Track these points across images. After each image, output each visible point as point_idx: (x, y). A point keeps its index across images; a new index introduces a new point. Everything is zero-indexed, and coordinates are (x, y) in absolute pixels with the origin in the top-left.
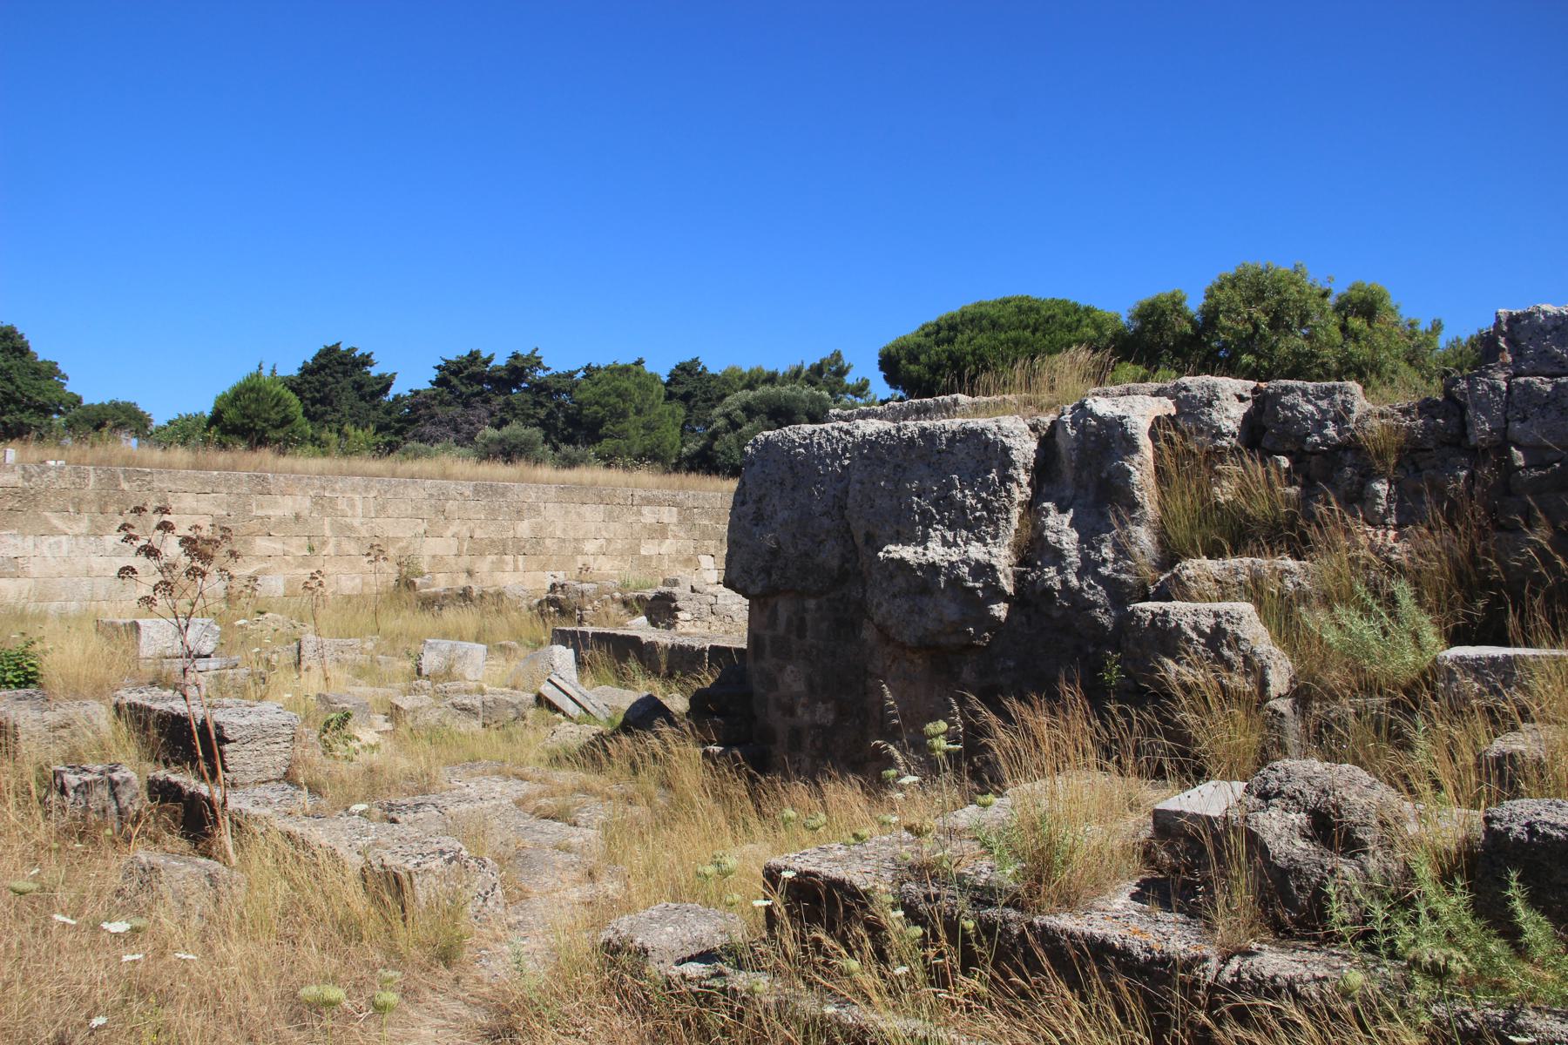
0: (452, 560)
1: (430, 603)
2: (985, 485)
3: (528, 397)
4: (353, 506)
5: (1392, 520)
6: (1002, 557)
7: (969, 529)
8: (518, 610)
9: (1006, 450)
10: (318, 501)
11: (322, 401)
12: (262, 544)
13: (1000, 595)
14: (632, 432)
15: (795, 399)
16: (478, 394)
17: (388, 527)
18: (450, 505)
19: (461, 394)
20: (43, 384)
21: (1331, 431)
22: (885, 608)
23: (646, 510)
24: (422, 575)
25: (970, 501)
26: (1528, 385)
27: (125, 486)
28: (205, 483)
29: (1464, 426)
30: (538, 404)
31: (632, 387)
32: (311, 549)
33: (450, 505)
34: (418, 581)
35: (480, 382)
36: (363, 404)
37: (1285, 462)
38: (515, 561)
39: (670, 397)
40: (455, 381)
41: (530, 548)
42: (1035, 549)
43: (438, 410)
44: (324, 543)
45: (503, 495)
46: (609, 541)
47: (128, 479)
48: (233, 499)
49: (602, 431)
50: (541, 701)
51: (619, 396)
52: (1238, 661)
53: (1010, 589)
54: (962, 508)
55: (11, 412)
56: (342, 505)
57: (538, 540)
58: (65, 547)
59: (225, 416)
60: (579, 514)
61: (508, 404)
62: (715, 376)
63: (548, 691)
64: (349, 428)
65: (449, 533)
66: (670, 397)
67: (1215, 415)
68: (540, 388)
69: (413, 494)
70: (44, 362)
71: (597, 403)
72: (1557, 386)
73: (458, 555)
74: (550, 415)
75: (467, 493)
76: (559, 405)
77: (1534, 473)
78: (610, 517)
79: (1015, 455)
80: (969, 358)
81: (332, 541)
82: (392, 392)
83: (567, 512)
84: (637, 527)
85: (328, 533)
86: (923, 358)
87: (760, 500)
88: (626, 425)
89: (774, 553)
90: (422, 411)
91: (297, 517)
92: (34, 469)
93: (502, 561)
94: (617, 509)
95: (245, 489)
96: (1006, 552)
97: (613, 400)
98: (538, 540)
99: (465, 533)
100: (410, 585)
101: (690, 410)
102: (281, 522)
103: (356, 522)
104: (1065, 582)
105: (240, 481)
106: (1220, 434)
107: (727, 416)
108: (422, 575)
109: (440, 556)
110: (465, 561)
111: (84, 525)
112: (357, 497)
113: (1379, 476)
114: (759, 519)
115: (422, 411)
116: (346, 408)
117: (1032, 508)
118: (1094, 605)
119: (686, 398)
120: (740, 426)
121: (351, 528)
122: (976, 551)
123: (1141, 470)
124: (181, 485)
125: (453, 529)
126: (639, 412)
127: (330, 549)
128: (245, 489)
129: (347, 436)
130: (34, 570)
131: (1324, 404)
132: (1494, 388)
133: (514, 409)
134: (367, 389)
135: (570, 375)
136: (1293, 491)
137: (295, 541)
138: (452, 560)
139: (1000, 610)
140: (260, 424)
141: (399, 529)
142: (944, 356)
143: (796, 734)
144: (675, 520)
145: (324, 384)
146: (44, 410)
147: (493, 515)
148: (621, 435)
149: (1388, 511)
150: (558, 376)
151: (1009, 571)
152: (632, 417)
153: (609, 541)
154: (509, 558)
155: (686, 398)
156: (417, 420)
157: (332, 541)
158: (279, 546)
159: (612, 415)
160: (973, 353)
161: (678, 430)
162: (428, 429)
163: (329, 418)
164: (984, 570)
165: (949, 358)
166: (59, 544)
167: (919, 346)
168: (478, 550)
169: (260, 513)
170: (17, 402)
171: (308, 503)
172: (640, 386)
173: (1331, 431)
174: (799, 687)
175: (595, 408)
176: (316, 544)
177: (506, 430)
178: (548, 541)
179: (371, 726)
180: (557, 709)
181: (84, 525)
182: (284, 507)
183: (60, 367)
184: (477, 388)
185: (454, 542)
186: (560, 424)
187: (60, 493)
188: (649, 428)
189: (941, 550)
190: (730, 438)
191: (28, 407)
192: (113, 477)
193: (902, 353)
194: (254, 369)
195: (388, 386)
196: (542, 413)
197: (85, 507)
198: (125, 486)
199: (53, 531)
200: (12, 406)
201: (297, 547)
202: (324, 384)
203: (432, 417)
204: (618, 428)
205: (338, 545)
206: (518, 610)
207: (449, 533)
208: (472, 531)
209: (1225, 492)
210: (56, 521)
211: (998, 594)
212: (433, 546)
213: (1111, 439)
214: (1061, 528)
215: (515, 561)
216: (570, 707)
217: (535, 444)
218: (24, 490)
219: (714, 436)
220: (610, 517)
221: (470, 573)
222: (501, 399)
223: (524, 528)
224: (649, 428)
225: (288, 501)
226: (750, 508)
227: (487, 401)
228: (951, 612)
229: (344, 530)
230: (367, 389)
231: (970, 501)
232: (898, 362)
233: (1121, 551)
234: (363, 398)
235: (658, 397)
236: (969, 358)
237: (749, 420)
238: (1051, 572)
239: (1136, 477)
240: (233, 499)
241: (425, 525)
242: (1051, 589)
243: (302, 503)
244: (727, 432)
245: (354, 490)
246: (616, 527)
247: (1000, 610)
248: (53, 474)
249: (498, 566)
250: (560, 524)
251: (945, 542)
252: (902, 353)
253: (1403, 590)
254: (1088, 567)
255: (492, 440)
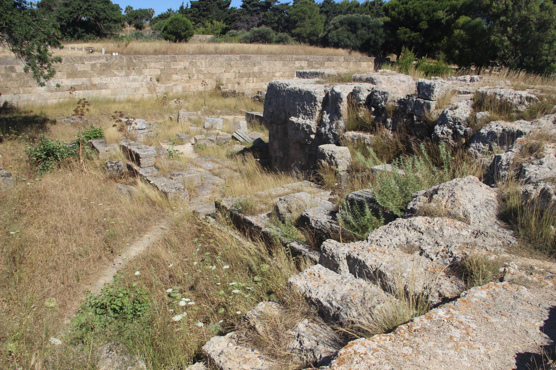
0: (233, 79)
1: (225, 95)
2: (311, 105)
3: (272, 12)
4: (202, 64)
5: (391, 128)
6: (313, 124)
7: (308, 115)
8: (248, 98)
9: (315, 98)
10: (191, 63)
11: (206, 10)
12: (175, 77)
13: (312, 133)
14: (307, 25)
15: (357, 19)
16: (256, 11)
17: (213, 70)
18: (232, 63)
19: (250, 11)
20: (115, 13)
21: (383, 104)
22: (291, 132)
23: (296, 62)
24: (223, 85)
25: (308, 109)
26: (419, 101)
27: (134, 61)
28: (157, 59)
29: (406, 108)
30: (275, 15)
31: (307, 9)
32: (189, 78)
33: (232, 63)
34: (221, 87)
35: (256, 6)
36: (221, 11)
37: (373, 109)
38: (253, 79)
39: (321, 12)
40: (248, 6)
41: (258, 76)
42: (321, 123)
43: (242, 17)
44: (193, 76)
45: (249, 59)
46: (284, 72)
47: (135, 59)
48: (165, 63)
49: (297, 25)
50: (233, 137)
51: (303, 12)
52: (334, 163)
53: (315, 132)
54: (306, 110)
55: (106, 23)
56: (198, 64)
57: (260, 73)
58: (119, 80)
59: (168, 28)
60: (274, 64)
61: (265, 15)
62: (338, 4)
63: (235, 135)
64: (215, 22)
65: (232, 71)
66: (321, 12)
67: (360, 95)
68: (276, 9)
69: (220, 60)
70: (115, 5)
71: (295, 15)
72: (424, 102)
73: (235, 78)
74: (279, 19)
75: (238, 58)
76: (282, 16)
77: (418, 123)
78: (284, 65)
79: (317, 99)
80: (411, 10)
81: (196, 75)
82: (231, 6)
83: (270, 64)
84: (293, 68)
85: (194, 72)
86: (396, 9)
87: (270, 99)
88: (304, 23)
89: (272, 113)
90: (237, 17)
91: (185, 68)
92: (109, 58)
93: (249, 80)
94: (287, 62)
95: (169, 60)
96: (315, 122)
97: (300, 14)
98: (260, 73)
99: (237, 71)
100: (219, 88)
101: (328, 17)
102: (180, 70)
103: (203, 69)
104: (325, 132)
105: (167, 58)
106: (360, 100)
107: (334, 24)
108: (223, 85)
109: (229, 78)
110: (237, 80)
111: (123, 73)
112: (203, 61)
113: (389, 117)
114: (270, 103)
115: (237, 17)
116: (214, 13)
117: (322, 113)
118: (330, 139)
119: (326, 12)
120: (338, 28)
121: (201, 71)
122: (308, 122)
123: (344, 107)
124: (150, 60)
125: (233, 70)
126: (310, 18)
127: (195, 77)
128: (169, 60)
129: (214, 24)
130: (111, 86)
131: (383, 96)
132: (413, 100)
133: (267, 17)
134: (222, 5)
135: (287, 4)
136: (374, 117)
137: (185, 75)
138: (233, 79)
139: (313, 136)
140: (179, 31)
141: (217, 70)
142: (403, 9)
143: (276, 157)
144: (306, 65)
145: (207, 5)
146: (116, 21)
147: (246, 65)
148: (303, 26)
149: (390, 126)
150: (282, 5)
151: (315, 127)
152: (307, 20)
153: (284, 72)
154: (251, 79)
155: (326, 12)
156: (235, 21)
157: (196, 75)
158: (180, 77)
159: (300, 19)
160: (413, 9)
161: (323, 24)
162: (239, 24)
163: (209, 16)
164: (309, 127)
165: (405, 10)
166: (117, 79)
167: (396, 5)
168: (241, 76)
169: (174, 67)
170: (108, 19)
171: (188, 64)
172: (310, 9)
173: (383, 104)
174: (277, 147)
175: (295, 17)
176: (191, 76)
177: (260, 28)
178: (264, 73)
179: (190, 142)
180: (237, 140)
181: (123, 73)
182: (181, 65)
183: (120, 6)
184: (255, 8)
185: (234, 74)
186: (283, 22)
187: (116, 64)
188: (313, 23)
189: (302, 120)
190: (334, 32)
191: (111, 21)
192: (131, 58)
193: (390, 7)
194: (181, 4)
195: (229, 4)
196: (276, 18)
197: (124, 68)
198: (134, 61)
199: (115, 75)
200: (106, 21)
201: (185, 77)
202: (207, 5)
203: (240, 19)
204: (302, 24)
205: (198, 76)
206: (248, 98)
207: (232, 71)
208: (239, 70)
209: (361, 114)
210: (116, 72)
211: (312, 133)
212: (227, 75)
213: (337, 97)
214: (326, 118)
215: (253, 79)
216: (241, 139)
217: (270, 33)
218: (107, 64)
219: (329, 31)
220: (284, 65)
221: (239, 84)
222: (263, 13)
223: (256, 69)
224: (313, 23)
225: (182, 63)
226: (268, 100)
227: (258, 14)
228: (303, 135)
229: (199, 72)
230: (222, 5)
231: (308, 109)
232: (388, 10)
233: (337, 127)
234: (220, 8)
235: (317, 13)
236: (411, 10)
237: (341, 26)
238: (323, 129)
239: (341, 108)
240: (165, 63)
241: (224, 69)
242: (322, 133)
243: (186, 64)
244: (333, 30)
245: (202, 59)
246: (287, 68)
247: (313, 136)
248: (114, 59)
249: (248, 81)
250: (268, 67)
251: (303, 118)
252: (390, 7)
253: (371, 150)
254: (330, 129)
255: (255, 32)
